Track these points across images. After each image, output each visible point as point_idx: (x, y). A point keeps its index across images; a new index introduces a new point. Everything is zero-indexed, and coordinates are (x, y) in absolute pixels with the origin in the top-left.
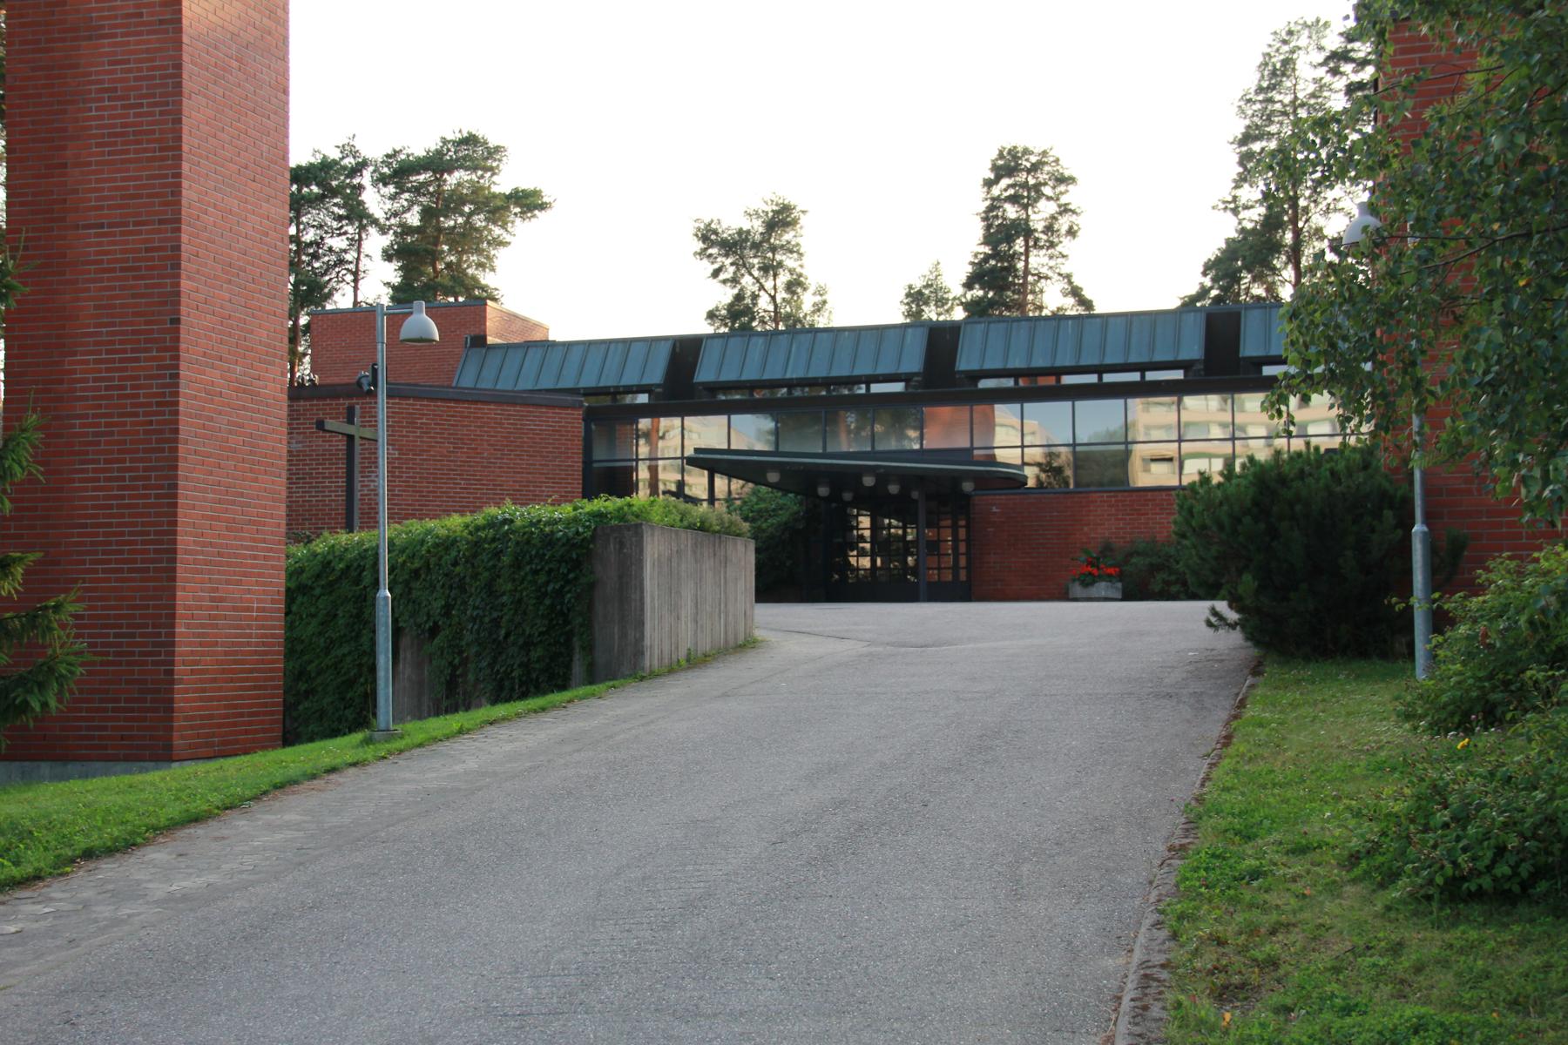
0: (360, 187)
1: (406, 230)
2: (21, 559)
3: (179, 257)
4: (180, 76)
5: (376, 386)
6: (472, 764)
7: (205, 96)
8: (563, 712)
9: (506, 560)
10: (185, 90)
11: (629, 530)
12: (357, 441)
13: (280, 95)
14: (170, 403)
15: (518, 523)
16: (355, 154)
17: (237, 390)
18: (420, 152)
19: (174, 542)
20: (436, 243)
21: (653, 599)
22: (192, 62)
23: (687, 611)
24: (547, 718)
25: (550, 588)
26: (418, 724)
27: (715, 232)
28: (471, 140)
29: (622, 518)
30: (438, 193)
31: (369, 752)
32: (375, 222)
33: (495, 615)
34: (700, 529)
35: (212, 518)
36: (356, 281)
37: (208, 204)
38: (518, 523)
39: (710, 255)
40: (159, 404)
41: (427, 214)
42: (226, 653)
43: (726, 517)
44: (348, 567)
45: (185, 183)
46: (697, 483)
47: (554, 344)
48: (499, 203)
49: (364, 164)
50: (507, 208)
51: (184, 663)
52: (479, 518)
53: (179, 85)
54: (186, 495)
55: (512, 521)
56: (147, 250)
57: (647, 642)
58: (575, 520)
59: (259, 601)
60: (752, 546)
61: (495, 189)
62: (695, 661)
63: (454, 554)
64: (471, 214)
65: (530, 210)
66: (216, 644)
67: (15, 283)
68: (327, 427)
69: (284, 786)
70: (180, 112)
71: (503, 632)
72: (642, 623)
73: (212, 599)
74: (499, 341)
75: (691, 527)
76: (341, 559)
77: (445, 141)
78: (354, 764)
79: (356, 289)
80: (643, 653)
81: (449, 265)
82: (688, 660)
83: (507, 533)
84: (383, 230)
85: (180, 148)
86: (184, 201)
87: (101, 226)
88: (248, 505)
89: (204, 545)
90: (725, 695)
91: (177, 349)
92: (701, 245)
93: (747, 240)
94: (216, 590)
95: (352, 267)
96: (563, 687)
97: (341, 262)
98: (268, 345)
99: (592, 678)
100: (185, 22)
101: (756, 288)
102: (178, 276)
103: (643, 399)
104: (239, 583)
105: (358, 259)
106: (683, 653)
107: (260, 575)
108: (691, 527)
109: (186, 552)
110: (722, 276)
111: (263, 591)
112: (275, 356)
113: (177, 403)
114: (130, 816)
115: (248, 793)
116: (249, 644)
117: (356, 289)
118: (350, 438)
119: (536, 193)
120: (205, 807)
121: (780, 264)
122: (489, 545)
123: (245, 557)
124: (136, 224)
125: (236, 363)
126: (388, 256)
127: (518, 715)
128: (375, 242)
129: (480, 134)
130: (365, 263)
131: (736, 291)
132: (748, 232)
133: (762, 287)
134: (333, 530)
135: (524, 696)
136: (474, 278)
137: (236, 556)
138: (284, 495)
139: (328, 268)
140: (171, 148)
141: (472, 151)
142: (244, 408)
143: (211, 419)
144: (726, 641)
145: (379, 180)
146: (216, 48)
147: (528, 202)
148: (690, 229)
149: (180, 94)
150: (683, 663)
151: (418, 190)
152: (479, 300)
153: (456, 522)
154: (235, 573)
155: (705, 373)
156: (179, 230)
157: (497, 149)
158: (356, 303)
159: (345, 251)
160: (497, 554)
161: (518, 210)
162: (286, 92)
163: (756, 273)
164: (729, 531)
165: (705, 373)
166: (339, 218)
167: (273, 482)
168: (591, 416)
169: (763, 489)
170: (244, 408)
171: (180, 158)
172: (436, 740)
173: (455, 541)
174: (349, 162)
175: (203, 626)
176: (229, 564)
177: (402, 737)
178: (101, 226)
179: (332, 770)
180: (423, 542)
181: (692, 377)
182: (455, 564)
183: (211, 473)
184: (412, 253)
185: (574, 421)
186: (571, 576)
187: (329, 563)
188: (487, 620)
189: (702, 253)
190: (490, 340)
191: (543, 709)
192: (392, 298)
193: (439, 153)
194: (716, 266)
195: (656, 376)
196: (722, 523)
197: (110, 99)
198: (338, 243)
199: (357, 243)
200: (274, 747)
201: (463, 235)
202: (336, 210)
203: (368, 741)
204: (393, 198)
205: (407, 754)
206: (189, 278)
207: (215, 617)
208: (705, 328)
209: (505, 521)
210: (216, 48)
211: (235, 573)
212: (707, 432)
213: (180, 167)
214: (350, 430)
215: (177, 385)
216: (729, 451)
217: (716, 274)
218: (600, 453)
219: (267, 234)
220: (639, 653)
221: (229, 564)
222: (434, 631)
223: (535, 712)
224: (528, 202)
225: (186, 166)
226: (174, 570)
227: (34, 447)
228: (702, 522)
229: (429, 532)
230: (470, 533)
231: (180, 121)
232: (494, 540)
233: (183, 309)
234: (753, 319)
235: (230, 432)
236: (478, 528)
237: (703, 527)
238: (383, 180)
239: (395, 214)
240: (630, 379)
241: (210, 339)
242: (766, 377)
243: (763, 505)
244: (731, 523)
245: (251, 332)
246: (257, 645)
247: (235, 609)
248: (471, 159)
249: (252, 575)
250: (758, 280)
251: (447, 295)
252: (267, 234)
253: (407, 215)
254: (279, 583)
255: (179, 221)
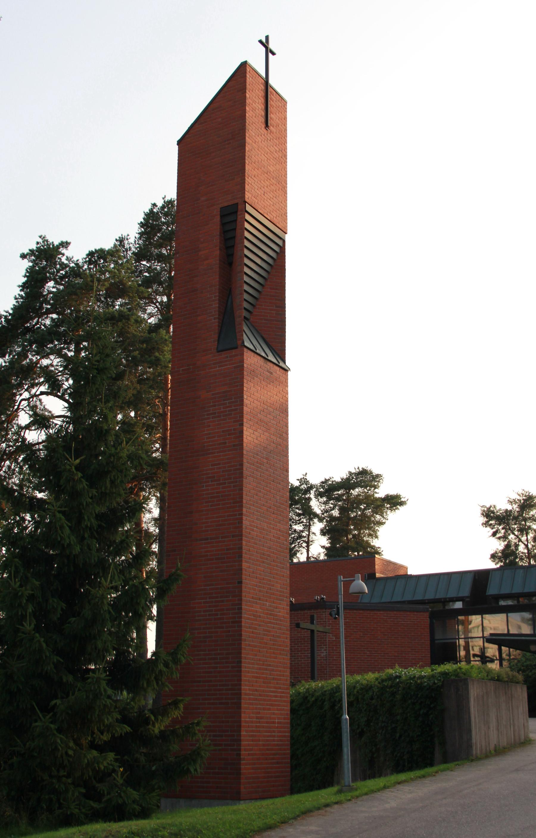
0: (310, 499)
1: (332, 519)
2: (182, 700)
3: (241, 552)
4: (242, 469)
5: (338, 615)
6: (393, 804)
7: (253, 477)
8: (434, 778)
9: (398, 697)
10: (244, 475)
11: (459, 683)
12: (316, 632)
13: (285, 473)
14: (238, 622)
15: (404, 677)
16: (306, 482)
17: (267, 614)
18: (338, 480)
19: (240, 689)
20: (348, 525)
21: (475, 718)
22: (248, 462)
23: (493, 724)
24: (427, 781)
25: (421, 712)
26: (363, 783)
27: (493, 512)
28: (364, 472)
29: (457, 675)
30: (348, 499)
31: (342, 797)
32: (316, 515)
33: (394, 725)
34: (498, 680)
35: (257, 677)
36: (308, 546)
37: (254, 526)
38: (404, 677)
39: (491, 524)
40: (233, 622)
41: (342, 510)
42: (264, 745)
43: (510, 673)
44: (316, 700)
45: (244, 518)
46: (492, 650)
47: (411, 576)
48: (379, 503)
49: (311, 487)
50: (383, 506)
51: (245, 750)
52: (383, 675)
53: (242, 473)
54: (246, 666)
55: (400, 677)
56: (227, 550)
57: (474, 741)
58: (433, 676)
59: (279, 718)
60: (525, 688)
61: (376, 496)
62: (499, 751)
63: (371, 694)
64: (365, 509)
65: (395, 506)
66: (259, 740)
67: (181, 573)
68: (301, 626)
69: (306, 813)
70: (242, 485)
71: (398, 735)
72: (470, 731)
73: (257, 718)
74: (382, 576)
75: (492, 679)
76: (313, 696)
77: (350, 473)
78: (336, 803)
79: (308, 551)
80: (471, 747)
81: (354, 536)
82: (495, 751)
83: (398, 683)
84: (321, 520)
85: (242, 502)
86: (244, 526)
87: (207, 539)
88: (273, 670)
89: (253, 690)
90: (517, 770)
91: (241, 596)
92: (485, 519)
93: (510, 515)
94: (259, 713)
95: (306, 539)
96: (432, 765)
97: (300, 537)
98: (281, 592)
99: (446, 760)
100: (245, 445)
101: (517, 541)
102: (241, 561)
103: (459, 605)
104: (269, 709)
105: (309, 535)
106: (492, 747)
107: (278, 705)
108: (492, 679)
109: (246, 694)
110: (498, 535)
111: (280, 714)
112: (283, 596)
113: (241, 622)
114: (241, 825)
115: (291, 816)
116: (274, 740)
117: (308, 551)
118: (312, 631)
119: (398, 497)
120: (273, 822)
121: (529, 528)
122: (390, 688)
123: (271, 696)
124: (222, 537)
125: (267, 601)
126: (323, 532)
127: (412, 779)
128: (317, 526)
129: (368, 469)
130: (312, 537)
131: (506, 543)
132: (511, 511)
133: (520, 540)
134: (307, 681)
135: (410, 769)
136: (367, 542)
137: (268, 696)
138: (289, 665)
139: (294, 540)
140: (238, 501)
141: (365, 478)
142: (270, 623)
143: (256, 629)
144: (515, 740)
145: (318, 495)
146: (257, 455)
147: (394, 501)
148: (479, 511)
149: (242, 477)
150: (493, 752)
151: (338, 499)
152: (372, 553)
153: (371, 676)
154: (267, 705)
155: (492, 590)
156: (242, 539)
157: (378, 476)
158: (308, 558)
159: (302, 531)
160: (393, 694)
161: (388, 506)
162: (287, 471)
163: (516, 533)
164: (512, 681)
165: (492, 590)
166: (299, 515)
167: (284, 659)
168: (433, 616)
169: (528, 654)
170: (270, 623)
171: (242, 506)
172: (373, 792)
173: (371, 687)
174: (304, 487)
175: (253, 731)
176: (265, 700)
177: (356, 790)
178: (207, 539)
179: (327, 805)
180: (354, 687)
181: (485, 592)
182: (372, 699)
183: (256, 655)
184: (333, 531)
185: (424, 619)
186: (432, 706)
187: (307, 697)
188: (389, 728)
189: (486, 524)
190: (378, 575)
191: (424, 776)
192: (326, 555)
193: (348, 479)
194: (494, 530)
195: (466, 592)
196: (508, 677)
197: (212, 481)
198: (298, 527)
199: (308, 527)
200: (282, 795)
201: (361, 520)
202: (297, 511)
203: (340, 792)
204: (325, 503)
205: (360, 798)
206: (246, 562)
207: (259, 727)
208: (491, 565)
209: (397, 677)
210: (257, 455)
211: (267, 705)
212: (496, 623)
213: (242, 510)
214: (312, 627)
215: (241, 613)
216: (509, 634)
217: (494, 534)
218: (438, 636)
219: (279, 538)
220: (469, 746)
221: (265, 700)
222: (362, 734)
223: (420, 777)
224: (394, 501)
225: (244, 510)
226: (240, 703)
227: (188, 648)
228: (498, 677)
229: (358, 682)
230: (379, 683)
231: (242, 489)
232: (391, 687)
233: (243, 576)
234: (516, 557)
235: (264, 635)
236: (383, 681)
237: (498, 679)
238: (319, 495)
239: (326, 511)
240: (452, 594)
241: (255, 590)
242: (526, 590)
243: (528, 663)
244: (513, 676)
245: (273, 586)
246: (278, 741)
247: (267, 723)
248: (364, 482)
249: (275, 705)
250: (517, 536)
251: (353, 551)
252: (279, 538)
253: (333, 512)
254: (287, 708)
255: (241, 535)
